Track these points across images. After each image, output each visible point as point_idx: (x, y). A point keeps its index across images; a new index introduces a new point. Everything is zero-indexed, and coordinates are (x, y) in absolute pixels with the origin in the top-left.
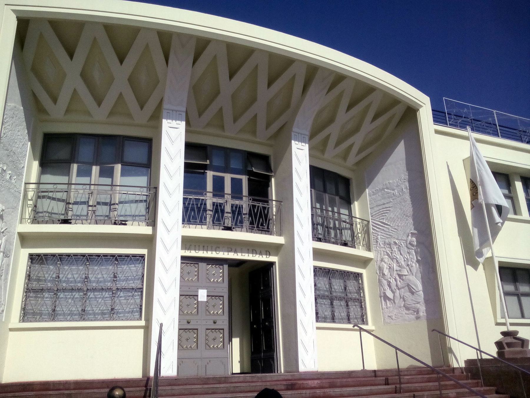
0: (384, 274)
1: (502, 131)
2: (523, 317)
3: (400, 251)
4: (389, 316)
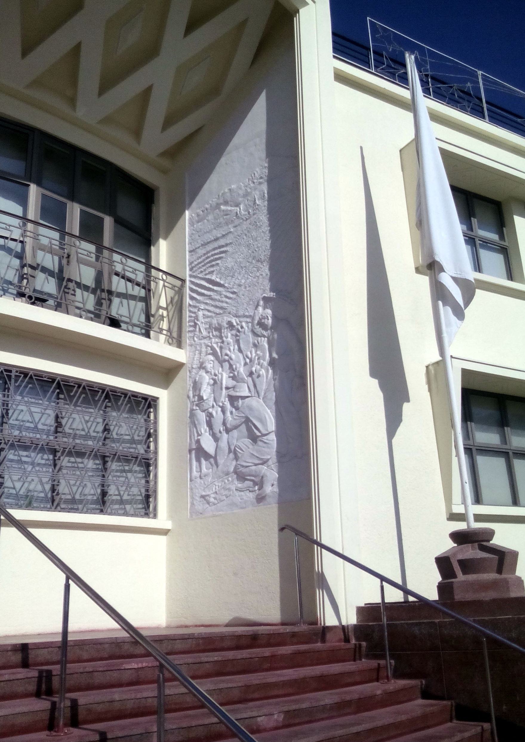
0: (201, 398)
1: (492, 114)
2: (515, 502)
3: (238, 342)
4: (203, 497)
